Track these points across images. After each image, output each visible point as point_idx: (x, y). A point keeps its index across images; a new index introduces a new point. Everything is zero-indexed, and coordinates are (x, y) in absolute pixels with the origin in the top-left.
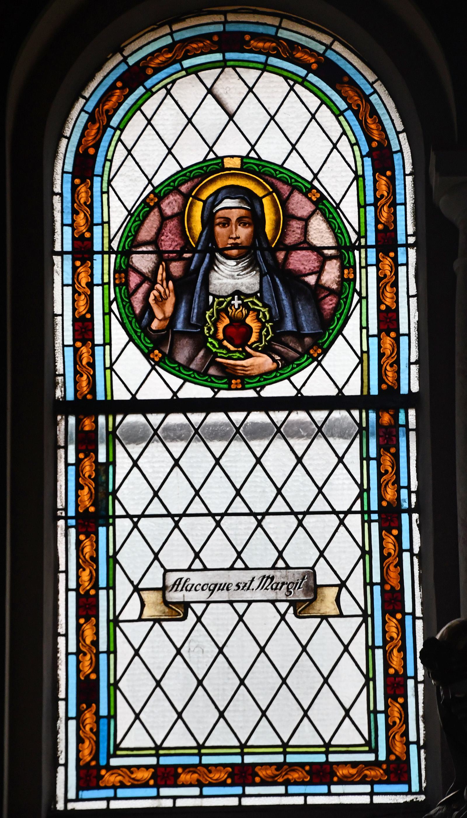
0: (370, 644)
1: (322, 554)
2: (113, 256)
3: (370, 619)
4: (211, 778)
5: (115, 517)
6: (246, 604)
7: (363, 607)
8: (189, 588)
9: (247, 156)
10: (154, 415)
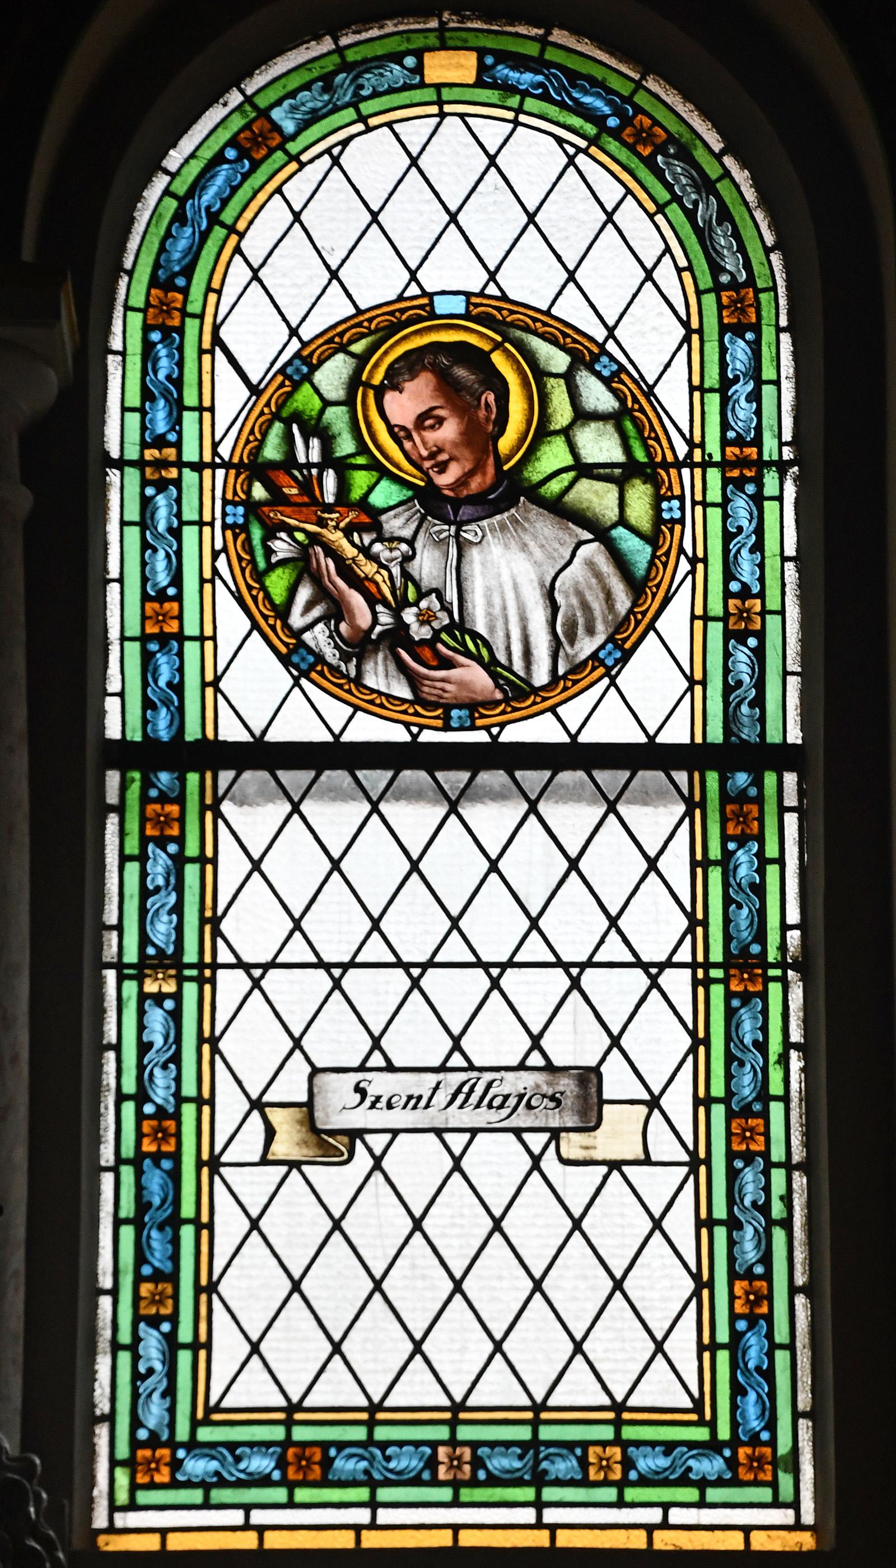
0: (703, 1214)
1: (615, 1041)
2: (220, 473)
3: (703, 1169)
4: (243, 1471)
5: (215, 966)
6: (467, 1136)
7: (691, 1147)
8: (495, 1103)
9: (482, 294)
10: (529, 774)
